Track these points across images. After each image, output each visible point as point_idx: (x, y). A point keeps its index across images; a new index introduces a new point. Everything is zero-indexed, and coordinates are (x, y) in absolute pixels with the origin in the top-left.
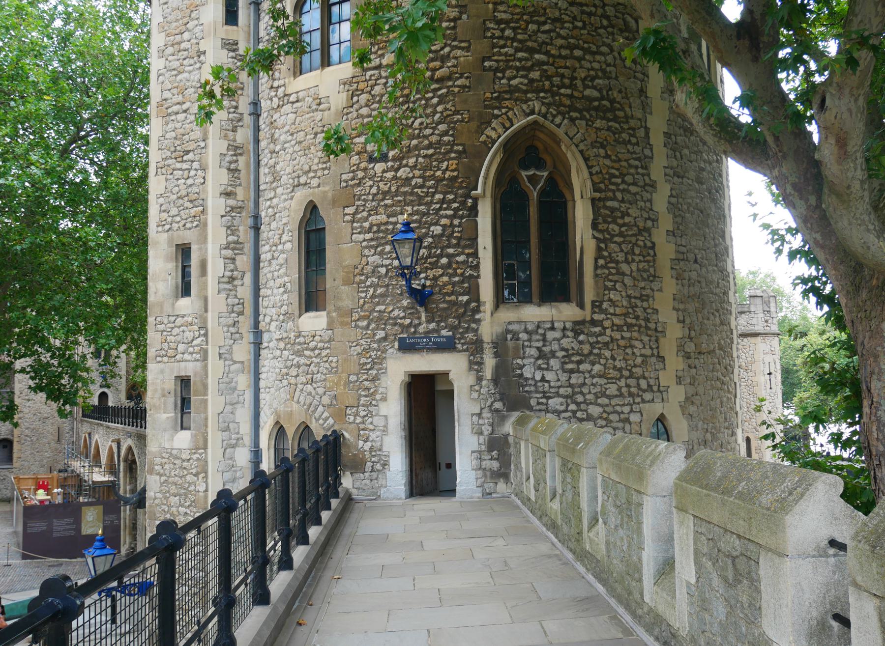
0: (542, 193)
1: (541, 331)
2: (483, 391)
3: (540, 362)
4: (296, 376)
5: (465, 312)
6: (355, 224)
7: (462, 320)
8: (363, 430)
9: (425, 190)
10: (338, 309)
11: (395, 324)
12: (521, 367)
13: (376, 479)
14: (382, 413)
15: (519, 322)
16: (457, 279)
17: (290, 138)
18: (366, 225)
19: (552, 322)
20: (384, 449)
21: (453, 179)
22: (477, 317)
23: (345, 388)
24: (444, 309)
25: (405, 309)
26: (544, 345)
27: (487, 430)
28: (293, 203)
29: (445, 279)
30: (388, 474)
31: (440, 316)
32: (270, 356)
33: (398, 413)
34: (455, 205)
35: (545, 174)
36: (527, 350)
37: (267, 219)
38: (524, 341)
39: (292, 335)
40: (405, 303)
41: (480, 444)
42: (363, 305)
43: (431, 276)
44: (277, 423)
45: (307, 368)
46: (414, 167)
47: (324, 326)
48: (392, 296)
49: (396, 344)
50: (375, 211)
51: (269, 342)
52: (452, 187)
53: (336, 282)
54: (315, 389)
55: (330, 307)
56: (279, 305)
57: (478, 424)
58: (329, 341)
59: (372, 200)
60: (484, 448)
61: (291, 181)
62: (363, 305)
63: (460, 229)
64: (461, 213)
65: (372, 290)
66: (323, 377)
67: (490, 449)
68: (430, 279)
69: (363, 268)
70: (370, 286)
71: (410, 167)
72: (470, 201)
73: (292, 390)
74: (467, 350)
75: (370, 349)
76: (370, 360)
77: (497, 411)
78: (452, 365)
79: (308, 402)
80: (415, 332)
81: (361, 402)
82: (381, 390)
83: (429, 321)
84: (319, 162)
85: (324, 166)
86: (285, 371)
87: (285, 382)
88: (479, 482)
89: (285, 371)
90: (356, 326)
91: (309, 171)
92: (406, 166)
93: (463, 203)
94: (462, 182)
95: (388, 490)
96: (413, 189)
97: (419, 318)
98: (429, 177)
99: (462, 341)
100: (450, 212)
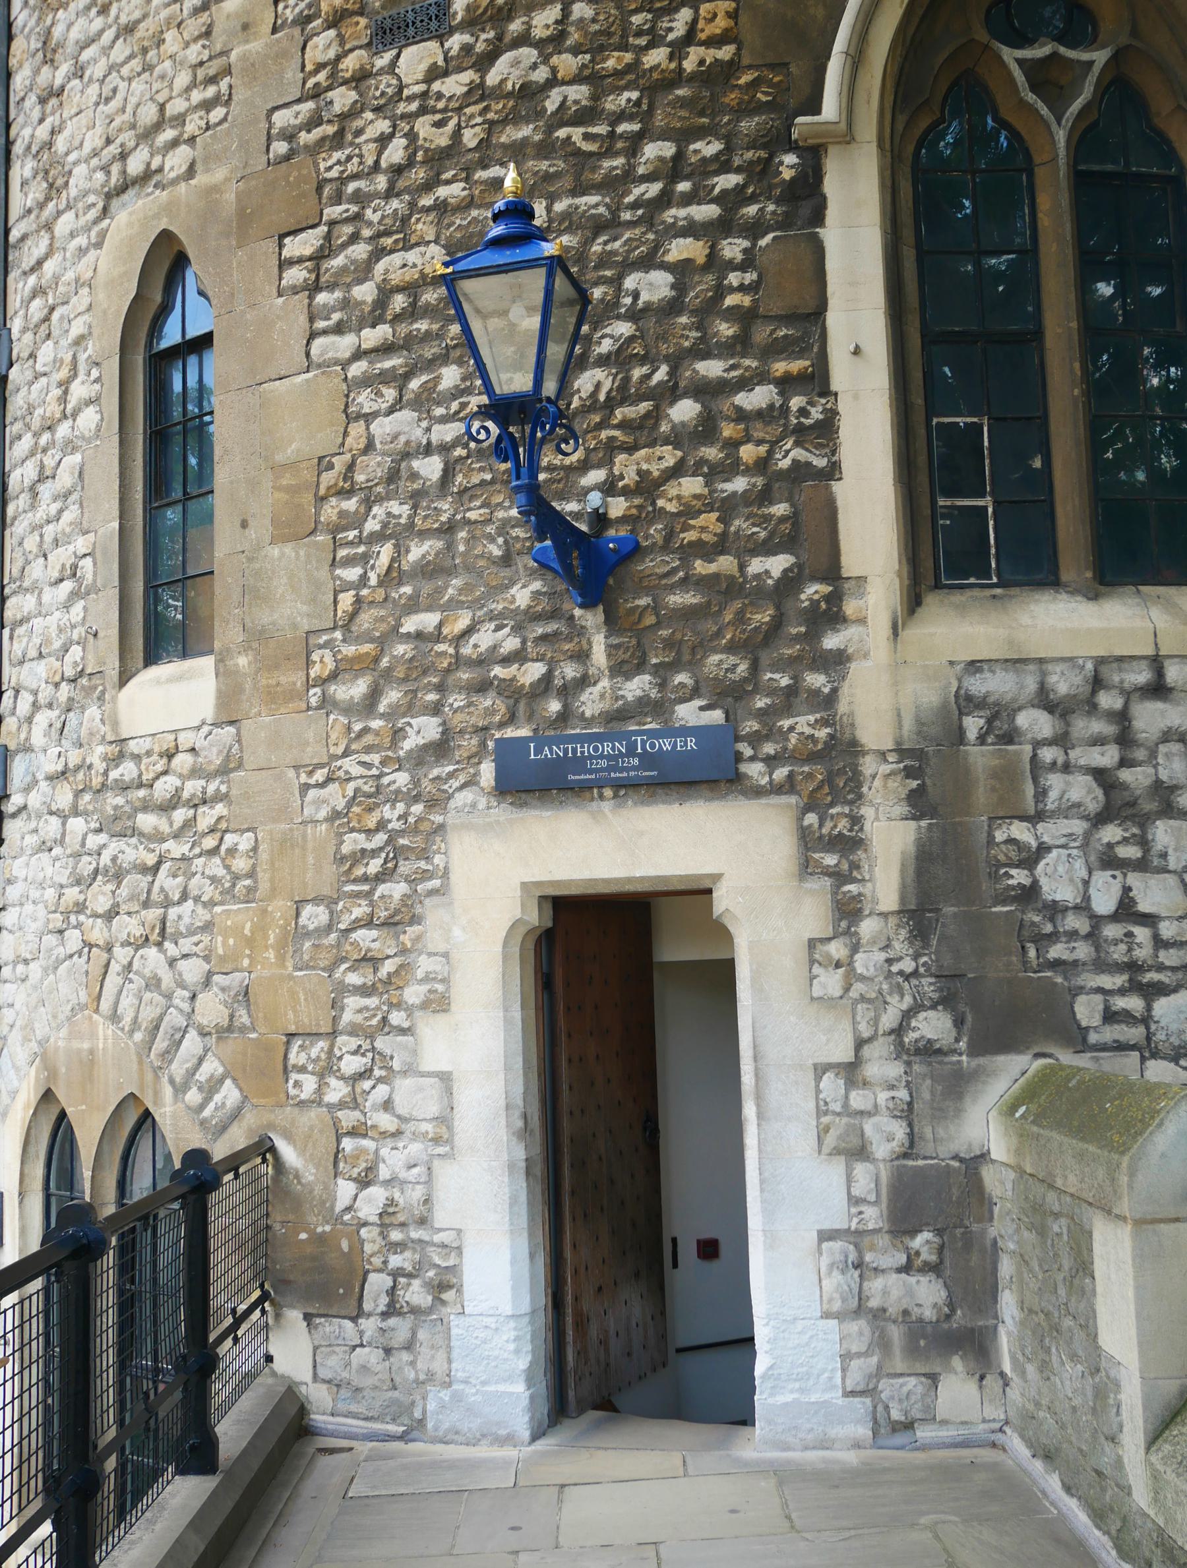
0: (1086, 140)
1: (1108, 700)
2: (865, 963)
3: (1111, 833)
4: (111, 915)
5: (778, 624)
6: (322, 298)
7: (765, 658)
8: (353, 1133)
9: (601, 129)
10: (257, 637)
11: (482, 687)
12: (1031, 858)
13: (409, 1346)
14: (427, 1065)
15: (1016, 663)
16: (739, 484)
17: (98, 23)
18: (365, 292)
19: (1157, 663)
20: (441, 1218)
21: (716, 76)
22: (831, 642)
23: (281, 958)
24: (688, 614)
25: (522, 620)
26: (1124, 763)
27: (885, 1135)
28: (104, 259)
29: (691, 486)
30: (458, 1326)
31: (669, 644)
32: (31, 840)
33: (500, 1064)
34: (727, 181)
35: (1100, 57)
36: (1055, 782)
37: (29, 336)
38: (1037, 744)
39: (97, 755)
40: (521, 596)
41: (854, 1201)
42: (353, 616)
43: (630, 478)
44: (48, 1096)
45: (144, 881)
46: (556, 41)
47: (206, 708)
48: (469, 569)
49: (487, 771)
50: (400, 234)
51: (27, 790)
52: (712, 108)
53: (251, 533)
54: (172, 962)
55: (227, 633)
56: (57, 644)
57: (847, 1111)
58: (224, 771)
59: (390, 193)
60: (873, 1217)
61: (100, 176)
62: (353, 616)
63: (750, 277)
64: (752, 210)
65: (385, 552)
66: (203, 915)
67: (902, 1222)
68: (626, 492)
69: (351, 467)
70: (378, 538)
71: (539, 44)
72: (790, 159)
73: (96, 969)
74: (789, 786)
75: (377, 795)
76: (380, 838)
77: (928, 1051)
78: (720, 850)
79: (148, 1014)
80: (564, 717)
81: (347, 1017)
82: (424, 965)
83: (620, 670)
84: (193, 85)
85: (211, 91)
86: (72, 894)
87: (73, 939)
88: (859, 1370)
89: (72, 894)
90: (326, 702)
91: (158, 127)
92: (524, 39)
93: (762, 171)
94: (754, 84)
95: (458, 1398)
96: (550, 129)
97: (582, 656)
98: (617, 73)
99: (769, 748)
100: (707, 212)
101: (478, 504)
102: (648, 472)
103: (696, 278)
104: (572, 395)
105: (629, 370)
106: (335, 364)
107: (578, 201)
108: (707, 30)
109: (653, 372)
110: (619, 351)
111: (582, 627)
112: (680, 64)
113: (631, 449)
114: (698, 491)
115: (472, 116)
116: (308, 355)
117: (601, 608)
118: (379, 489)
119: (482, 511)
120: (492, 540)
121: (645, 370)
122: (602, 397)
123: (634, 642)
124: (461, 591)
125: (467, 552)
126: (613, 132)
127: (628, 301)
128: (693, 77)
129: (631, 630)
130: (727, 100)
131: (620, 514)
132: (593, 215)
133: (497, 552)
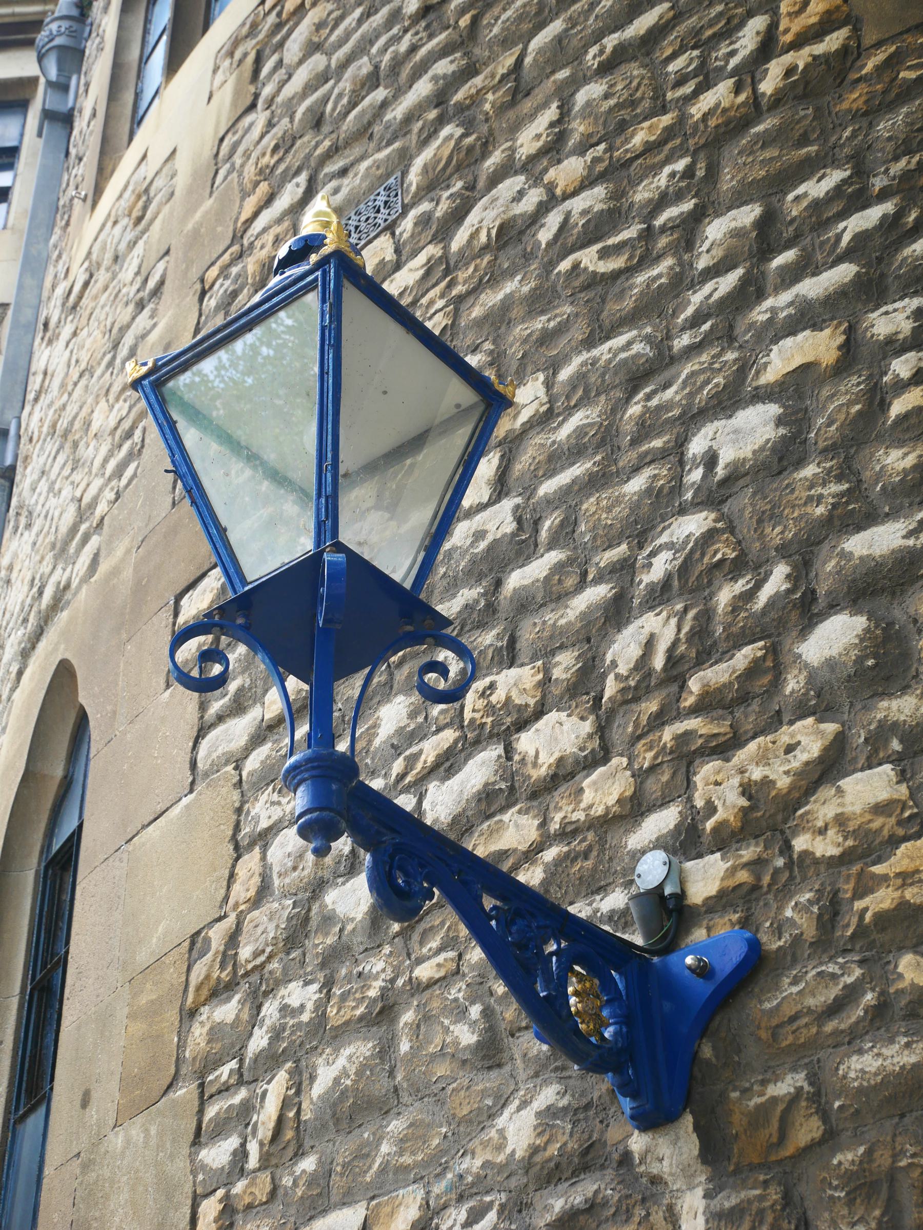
48: (419, 1093)
53: (93, 1112)
68: (724, 840)
69: (233, 939)
70: (270, 1060)
94: (892, 63)
98: (649, 148)
101: (434, 944)
102: (767, 783)
103: (826, 392)
104: (604, 676)
105: (712, 595)
106: (227, 763)
107: (595, 352)
108: (790, 27)
109: (758, 586)
110: (684, 569)
111: (656, 1180)
112: (754, 90)
113: (723, 749)
114: (883, 795)
115: (432, 302)
116: (193, 765)
117: (688, 1120)
118: (275, 965)
119: (440, 958)
120: (461, 1013)
121: (741, 585)
122: (658, 662)
123: (775, 1194)
124: (402, 1143)
125: (415, 1050)
126: (649, 228)
127: (697, 475)
128: (778, 100)
129: (764, 1166)
130: (845, 105)
131: (712, 889)
132: (625, 361)
133: (466, 1036)
